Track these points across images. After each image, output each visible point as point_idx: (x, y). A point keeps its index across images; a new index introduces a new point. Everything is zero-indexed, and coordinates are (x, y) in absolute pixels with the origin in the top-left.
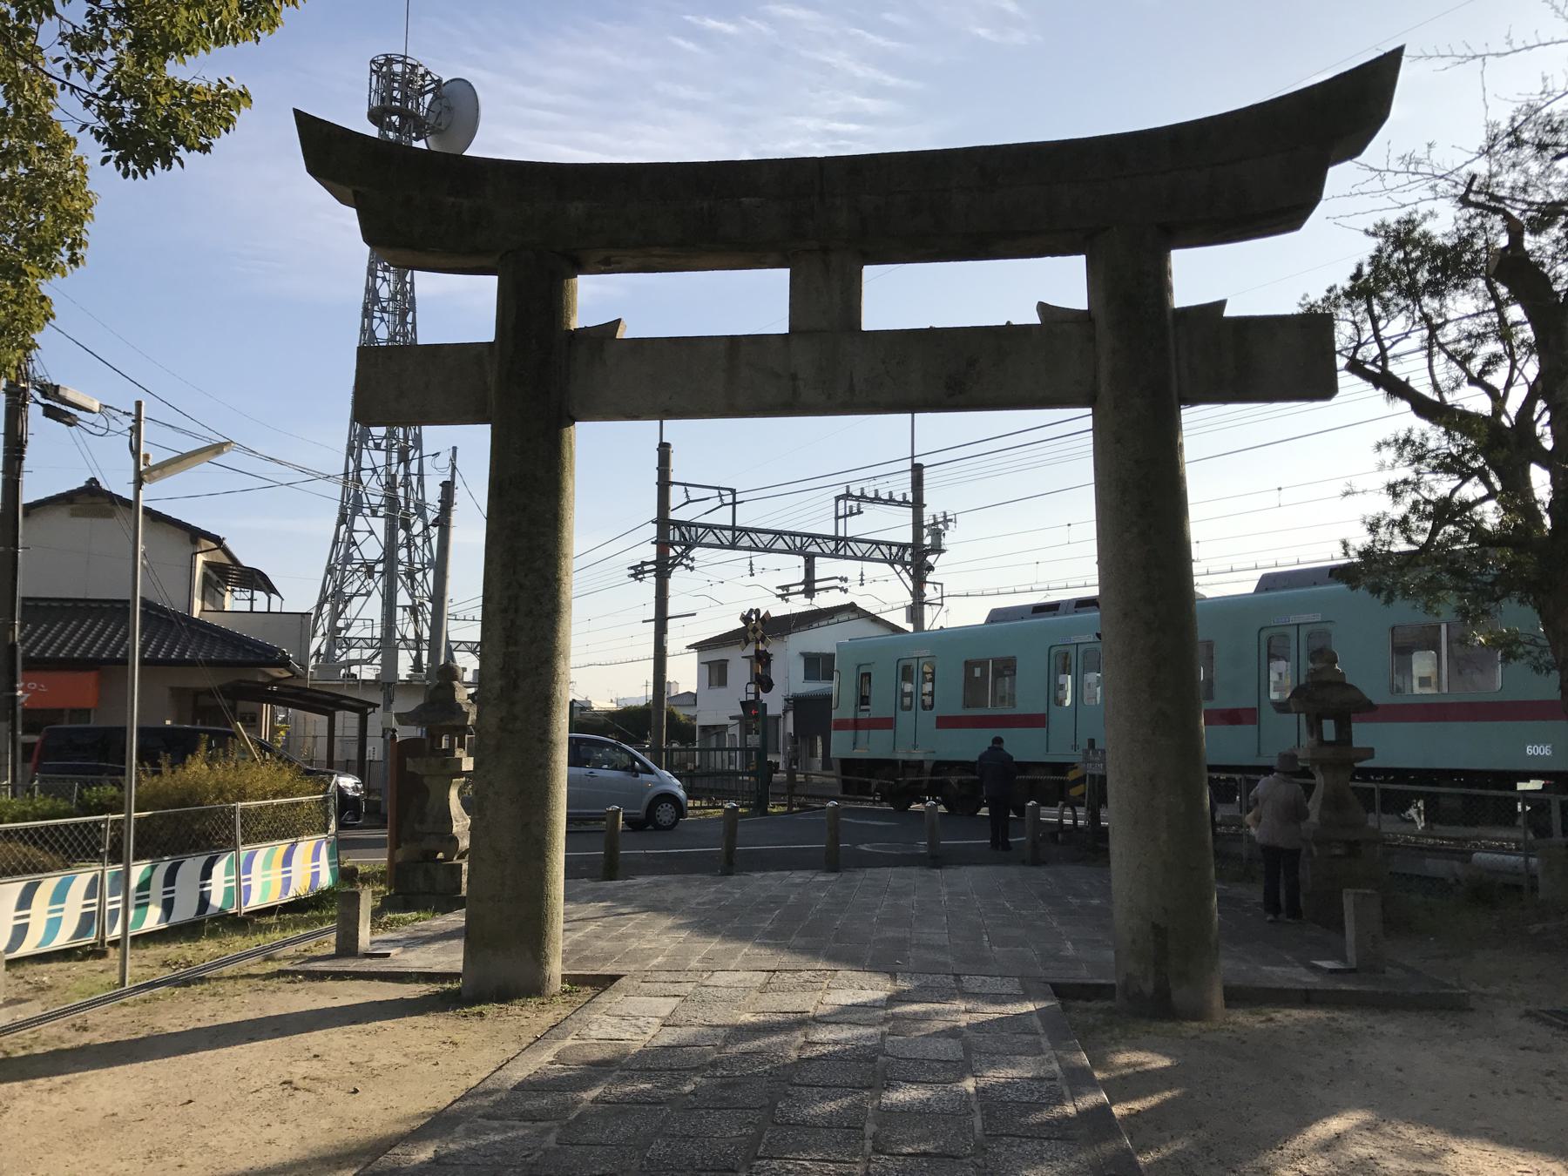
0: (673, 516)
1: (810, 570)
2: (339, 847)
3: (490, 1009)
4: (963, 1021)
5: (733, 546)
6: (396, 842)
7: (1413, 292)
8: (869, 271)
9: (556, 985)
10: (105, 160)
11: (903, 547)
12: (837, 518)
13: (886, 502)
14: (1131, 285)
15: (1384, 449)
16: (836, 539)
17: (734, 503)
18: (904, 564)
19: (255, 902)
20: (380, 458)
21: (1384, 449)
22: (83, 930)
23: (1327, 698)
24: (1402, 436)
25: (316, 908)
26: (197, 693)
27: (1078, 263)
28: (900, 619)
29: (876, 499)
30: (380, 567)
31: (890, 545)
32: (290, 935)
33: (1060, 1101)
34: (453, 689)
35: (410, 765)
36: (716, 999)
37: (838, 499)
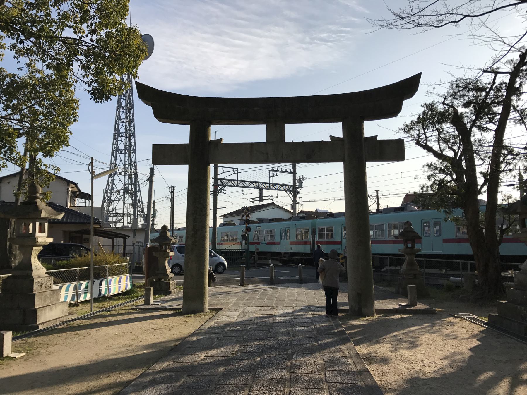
0: (219, 177)
1: (261, 193)
2: (132, 279)
3: (193, 315)
4: (311, 316)
5: (237, 186)
6: (148, 276)
7: (433, 124)
8: (286, 125)
9: (207, 310)
10: (91, 99)
11: (290, 186)
12: (269, 177)
13: (284, 172)
14: (353, 130)
15: (425, 167)
16: (269, 183)
17: (238, 173)
18: (290, 192)
19: (112, 293)
20: (122, 156)
21: (425, 167)
22: (72, 299)
23: (409, 236)
24: (429, 163)
25: (128, 295)
26: (71, 232)
27: (340, 124)
28: (289, 208)
29: (282, 171)
30: (122, 191)
31: (286, 185)
32: (128, 301)
33: (334, 329)
34: (166, 233)
35: (155, 254)
36: (249, 312)
37: (270, 171)
